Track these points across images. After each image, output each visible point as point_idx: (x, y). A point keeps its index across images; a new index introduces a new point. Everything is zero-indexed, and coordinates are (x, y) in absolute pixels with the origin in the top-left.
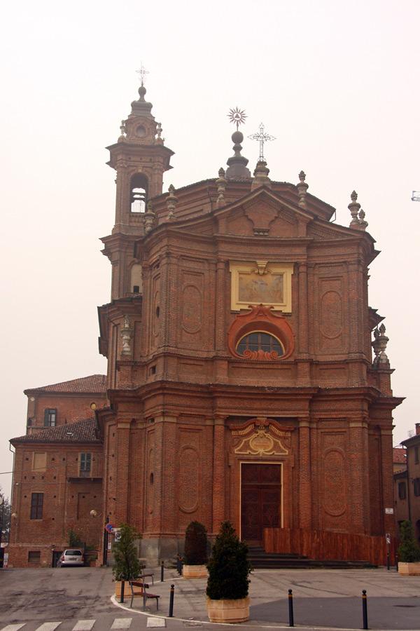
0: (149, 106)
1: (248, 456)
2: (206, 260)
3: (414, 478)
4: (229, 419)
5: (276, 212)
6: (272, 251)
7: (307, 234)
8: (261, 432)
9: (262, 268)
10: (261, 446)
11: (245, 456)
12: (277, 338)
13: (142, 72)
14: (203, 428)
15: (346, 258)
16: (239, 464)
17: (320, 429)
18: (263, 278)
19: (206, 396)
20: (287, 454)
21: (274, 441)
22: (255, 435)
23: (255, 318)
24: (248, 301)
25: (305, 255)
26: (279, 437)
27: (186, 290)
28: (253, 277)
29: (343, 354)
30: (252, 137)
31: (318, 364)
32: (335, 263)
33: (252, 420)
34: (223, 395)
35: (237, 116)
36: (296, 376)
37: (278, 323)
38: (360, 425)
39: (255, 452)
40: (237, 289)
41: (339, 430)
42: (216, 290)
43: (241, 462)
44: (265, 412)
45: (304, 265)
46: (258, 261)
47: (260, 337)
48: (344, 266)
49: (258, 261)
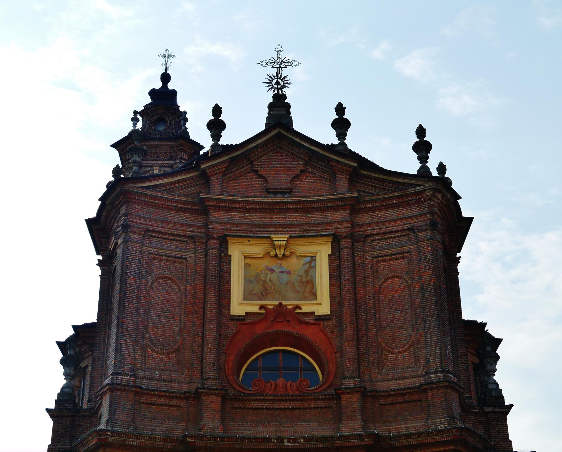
0: (174, 93)
3: (259, 310)
6: (294, 218)
7: (350, 190)
9: (280, 246)
15: (413, 222)
18: (286, 265)
24: (260, 299)
25: (347, 221)
27: (155, 284)
28: (267, 262)
29: (419, 376)
30: (264, 63)
31: (376, 395)
32: (397, 231)
35: (277, 83)
36: (338, 419)
37: (308, 333)
40: (242, 282)
42: (205, 283)
45: (346, 237)
46: (272, 236)
47: (281, 356)
48: (411, 235)
49: (272, 236)
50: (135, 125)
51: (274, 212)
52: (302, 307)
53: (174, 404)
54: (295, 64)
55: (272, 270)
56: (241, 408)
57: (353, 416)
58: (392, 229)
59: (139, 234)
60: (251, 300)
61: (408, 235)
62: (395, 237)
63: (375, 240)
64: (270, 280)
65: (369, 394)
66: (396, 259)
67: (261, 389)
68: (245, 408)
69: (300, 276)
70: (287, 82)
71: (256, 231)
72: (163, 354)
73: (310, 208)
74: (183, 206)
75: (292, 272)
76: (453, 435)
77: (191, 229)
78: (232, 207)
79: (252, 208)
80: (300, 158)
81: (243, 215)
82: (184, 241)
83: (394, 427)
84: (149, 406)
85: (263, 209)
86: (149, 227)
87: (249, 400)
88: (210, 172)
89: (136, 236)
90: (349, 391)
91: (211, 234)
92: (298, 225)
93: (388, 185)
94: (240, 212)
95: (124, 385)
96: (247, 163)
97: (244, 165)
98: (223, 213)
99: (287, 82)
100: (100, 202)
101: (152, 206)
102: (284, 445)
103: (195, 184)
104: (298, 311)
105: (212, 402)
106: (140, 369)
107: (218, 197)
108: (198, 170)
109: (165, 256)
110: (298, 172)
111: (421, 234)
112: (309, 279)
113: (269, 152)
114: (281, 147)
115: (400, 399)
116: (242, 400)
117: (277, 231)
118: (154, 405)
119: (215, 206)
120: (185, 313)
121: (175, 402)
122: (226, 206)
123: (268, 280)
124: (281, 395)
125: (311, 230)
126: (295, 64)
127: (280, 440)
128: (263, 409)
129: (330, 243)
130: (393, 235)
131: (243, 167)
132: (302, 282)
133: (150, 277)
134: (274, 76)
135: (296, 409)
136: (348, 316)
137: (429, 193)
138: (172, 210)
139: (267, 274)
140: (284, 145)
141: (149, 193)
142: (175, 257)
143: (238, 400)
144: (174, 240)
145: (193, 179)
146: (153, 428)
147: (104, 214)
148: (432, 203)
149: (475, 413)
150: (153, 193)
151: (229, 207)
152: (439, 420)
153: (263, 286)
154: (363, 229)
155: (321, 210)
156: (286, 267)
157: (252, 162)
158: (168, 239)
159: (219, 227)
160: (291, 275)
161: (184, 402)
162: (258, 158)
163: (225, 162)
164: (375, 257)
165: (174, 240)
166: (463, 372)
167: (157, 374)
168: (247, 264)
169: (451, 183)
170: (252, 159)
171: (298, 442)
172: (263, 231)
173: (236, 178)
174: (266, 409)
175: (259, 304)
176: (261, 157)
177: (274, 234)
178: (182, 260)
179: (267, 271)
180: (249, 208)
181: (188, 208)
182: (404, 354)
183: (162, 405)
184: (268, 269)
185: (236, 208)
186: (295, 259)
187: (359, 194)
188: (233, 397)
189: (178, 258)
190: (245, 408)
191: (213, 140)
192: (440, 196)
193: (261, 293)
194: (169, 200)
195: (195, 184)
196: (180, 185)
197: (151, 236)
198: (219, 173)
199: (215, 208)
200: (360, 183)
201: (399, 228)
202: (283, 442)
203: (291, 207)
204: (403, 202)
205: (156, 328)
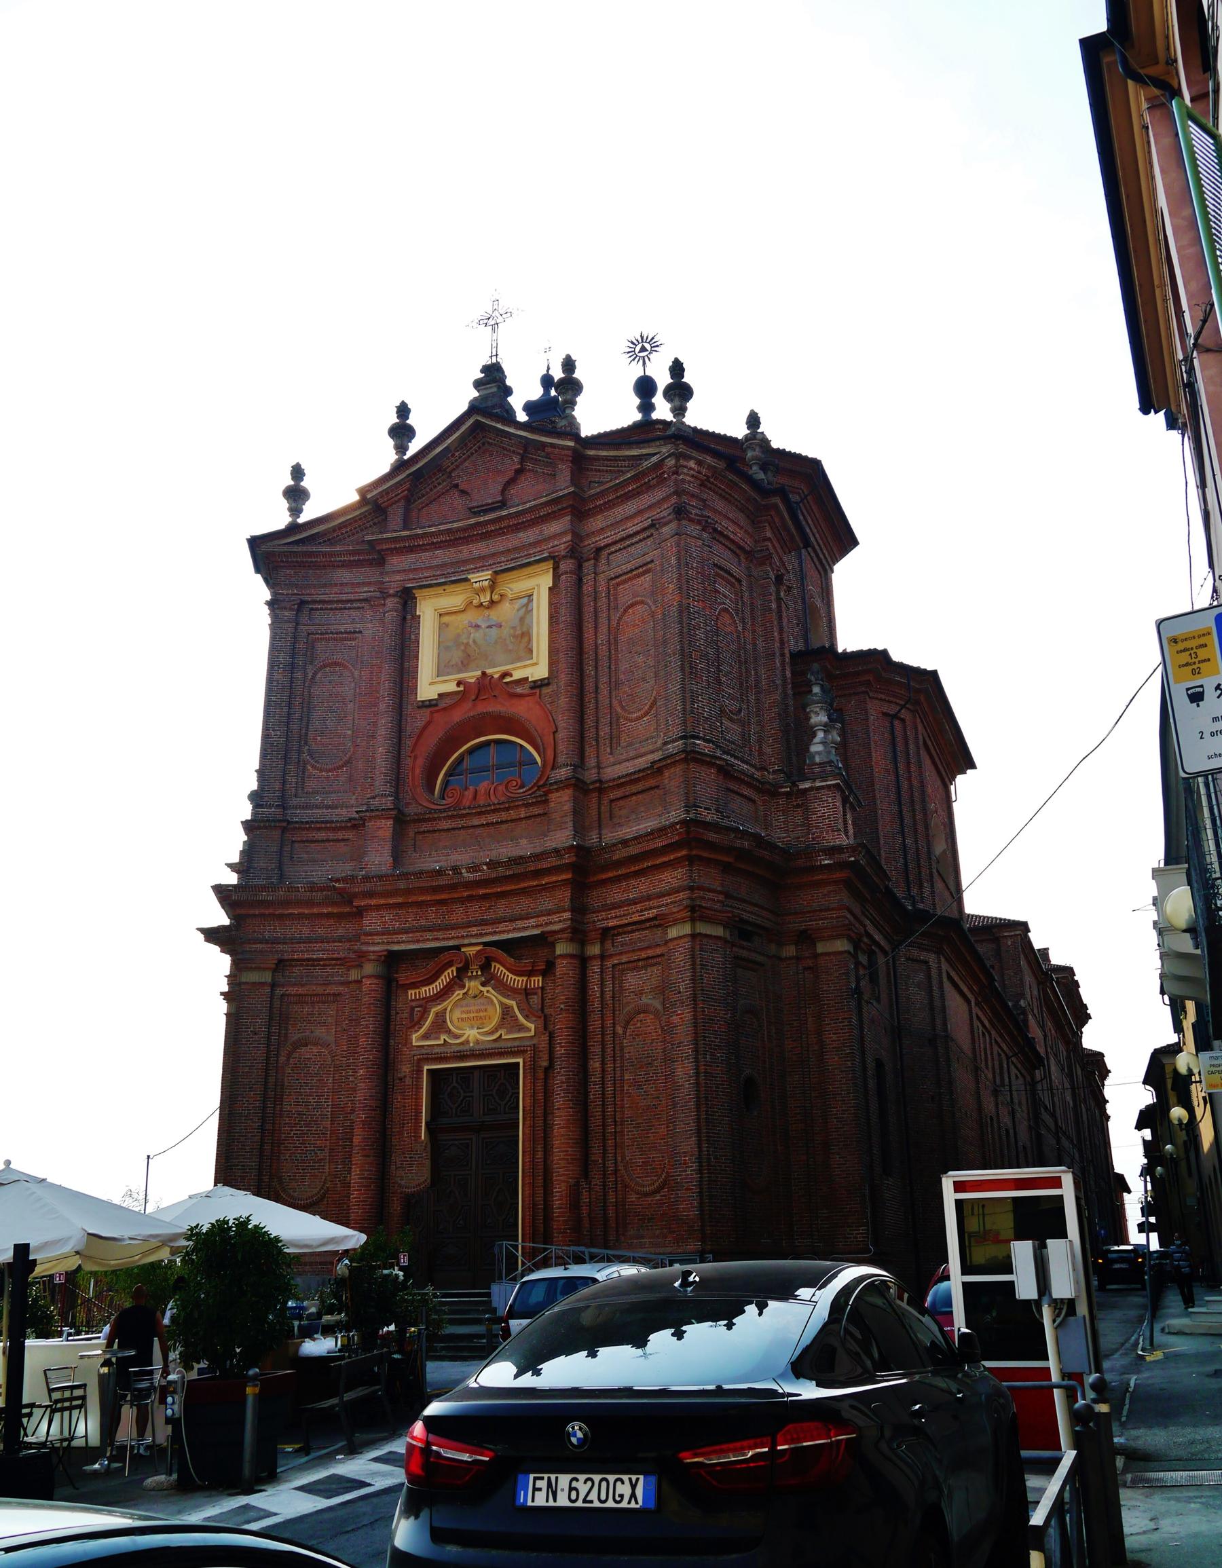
2: (365, 600)
4: (393, 960)
8: (473, 985)
9: (483, 589)
11: (437, 1050)
12: (482, 739)
13: (491, 322)
15: (654, 513)
16: (420, 1071)
17: (611, 956)
18: (495, 615)
20: (532, 1033)
21: (501, 1003)
22: (459, 993)
24: (460, 671)
27: (319, 675)
30: (475, 325)
31: (601, 788)
33: (444, 958)
34: (373, 902)
35: (643, 349)
37: (523, 710)
38: (686, 929)
39: (456, 1037)
41: (650, 953)
43: (426, 1068)
44: (475, 930)
45: (565, 557)
46: (469, 577)
51: (472, 541)
53: (340, 838)
55: (477, 626)
56: (428, 832)
58: (631, 531)
59: (291, 609)
60: (449, 674)
61: (652, 535)
62: (637, 542)
63: (613, 553)
64: (474, 641)
65: (591, 787)
66: (638, 576)
68: (434, 831)
69: (514, 628)
71: (448, 573)
72: (329, 771)
73: (519, 524)
74: (352, 558)
75: (503, 624)
76: (679, 834)
77: (366, 589)
79: (441, 541)
80: (514, 452)
82: (359, 608)
85: (456, 539)
87: (439, 819)
89: (286, 614)
90: (555, 787)
91: (386, 591)
92: (502, 553)
94: (426, 550)
95: (268, 821)
96: (444, 477)
97: (439, 480)
101: (309, 566)
102: (463, 877)
103: (371, 523)
104: (508, 679)
105: (380, 828)
109: (332, 633)
110: (511, 474)
111: (665, 530)
112: (525, 629)
113: (472, 454)
114: (489, 443)
115: (634, 788)
116: (430, 820)
117: (476, 568)
119: (390, 549)
120: (360, 708)
121: (341, 835)
122: (405, 547)
124: (469, 808)
125: (521, 557)
127: (456, 870)
128: (459, 829)
130: (635, 540)
131: (439, 484)
132: (515, 636)
133: (310, 667)
134: (637, 341)
135: (502, 822)
136: (563, 676)
137: (671, 462)
138: (338, 566)
140: (490, 438)
141: (295, 549)
143: (425, 820)
144: (345, 608)
145: (365, 516)
148: (681, 477)
149: (786, 794)
150: (305, 549)
151: (409, 546)
153: (464, 651)
154: (594, 540)
155: (534, 524)
156: (495, 618)
158: (336, 609)
159: (398, 578)
162: (457, 466)
163: (405, 483)
164: (612, 579)
165: (345, 608)
167: (318, 799)
168: (444, 623)
171: (480, 871)
172: (457, 572)
173: (431, 502)
174: (463, 827)
175: (454, 680)
176: (462, 463)
177: (473, 573)
178: (357, 635)
180: (437, 542)
181: (359, 560)
182: (645, 719)
183: (323, 841)
184: (471, 626)
185: (419, 545)
186: (507, 604)
188: (416, 817)
190: (434, 831)
191: (396, 454)
192: (692, 464)
193: (462, 662)
195: (371, 523)
197: (312, 609)
198: (400, 499)
200: (592, 470)
201: (638, 528)
202: (461, 873)
204: (642, 485)
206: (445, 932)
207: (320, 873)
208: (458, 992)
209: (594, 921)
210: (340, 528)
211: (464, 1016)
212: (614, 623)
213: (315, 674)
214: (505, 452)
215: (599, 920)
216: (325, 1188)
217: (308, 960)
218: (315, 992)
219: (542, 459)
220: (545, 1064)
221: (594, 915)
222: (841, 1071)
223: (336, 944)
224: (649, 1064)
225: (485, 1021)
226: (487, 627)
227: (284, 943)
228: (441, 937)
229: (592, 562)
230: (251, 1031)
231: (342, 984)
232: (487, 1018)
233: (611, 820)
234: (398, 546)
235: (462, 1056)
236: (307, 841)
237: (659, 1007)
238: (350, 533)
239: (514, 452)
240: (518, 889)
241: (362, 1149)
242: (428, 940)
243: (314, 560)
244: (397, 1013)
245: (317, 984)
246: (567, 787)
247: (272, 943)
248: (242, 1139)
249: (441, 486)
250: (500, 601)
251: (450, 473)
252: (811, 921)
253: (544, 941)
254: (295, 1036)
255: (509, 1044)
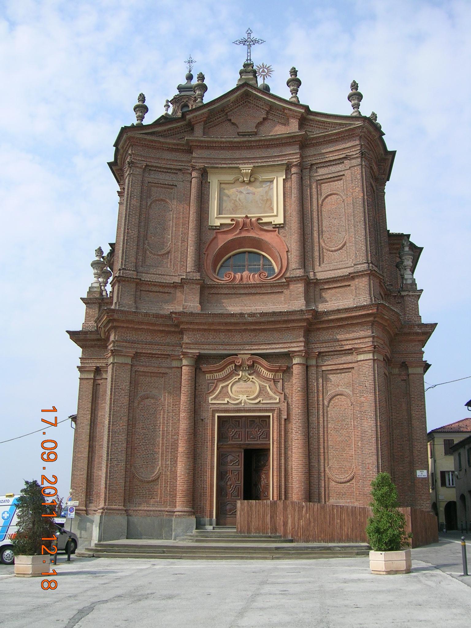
1: (226, 406)
2: (180, 170)
5: (264, 112)
9: (246, 174)
10: (242, 393)
11: (223, 406)
14: (167, 371)
16: (213, 416)
19: (173, 329)
20: (277, 401)
23: (240, 233)
26: (268, 380)
27: (153, 205)
30: (237, 42)
34: (191, 327)
43: (217, 415)
49: (240, 166)
50: (167, 110)
52: (263, 219)
53: (166, 291)
54: (261, 42)
57: (299, 297)
59: (141, 168)
64: (239, 199)
67: (231, 278)
68: (218, 294)
70: (270, 70)
73: (269, 145)
75: (256, 193)
77: (180, 164)
78: (211, 146)
79: (226, 146)
80: (263, 109)
81: (218, 152)
83: (329, 305)
84: (147, 292)
86: (148, 163)
88: (194, 121)
90: (295, 279)
91: (194, 166)
93: (328, 125)
97: (221, 116)
98: (203, 151)
99: (270, 70)
100: (115, 148)
101: (150, 147)
103: (183, 131)
106: (141, 266)
107: (199, 139)
108: (185, 120)
113: (239, 105)
114: (248, 102)
118: (151, 292)
121: (166, 290)
123: (238, 200)
126: (261, 42)
129: (285, 170)
131: (220, 117)
139: (237, 195)
142: (168, 185)
144: (168, 172)
146: (150, 308)
147: (119, 157)
152: (363, 299)
157: (227, 113)
160: (255, 195)
161: (173, 290)
162: (231, 110)
166: (386, 266)
169: (380, 127)
170: (226, 111)
175: (230, 217)
176: (233, 109)
178: (173, 187)
179: (237, 193)
180: (223, 147)
183: (157, 292)
186: (258, 183)
187: (306, 132)
189: (171, 185)
190: (218, 294)
193: (233, 209)
194: (163, 143)
195: (183, 131)
196: (172, 132)
197: (150, 170)
198: (201, 121)
199: (198, 147)
200: (308, 125)
203: (255, 144)
204: (340, 137)
205: (153, 236)
206: (230, 346)
207: (156, 309)
208: (235, 377)
209: (313, 348)
210: (168, 130)
211: (238, 390)
212: (320, 202)
213: (151, 203)
214: (258, 108)
215: (315, 348)
216: (159, 473)
217: (150, 354)
218: (153, 371)
219: (279, 115)
220: (285, 417)
221: (313, 345)
222: (420, 429)
223: (165, 347)
224: (343, 420)
225: (250, 393)
226: (247, 193)
227: (138, 344)
228: (228, 349)
229: (309, 169)
230: (120, 389)
231: (168, 368)
232: (252, 392)
233: (320, 299)
234: (202, 145)
235: (238, 411)
236: (148, 291)
237: (351, 393)
238: (172, 134)
239: (263, 109)
240: (274, 328)
241: (186, 454)
242: (221, 349)
243: (154, 144)
244: (199, 386)
245: (154, 367)
246: (301, 280)
247: (132, 343)
248: (117, 445)
249: (221, 119)
250: (254, 182)
251: (227, 113)
252: (406, 358)
253: (288, 356)
254: (331, 393)
255: (265, 406)
